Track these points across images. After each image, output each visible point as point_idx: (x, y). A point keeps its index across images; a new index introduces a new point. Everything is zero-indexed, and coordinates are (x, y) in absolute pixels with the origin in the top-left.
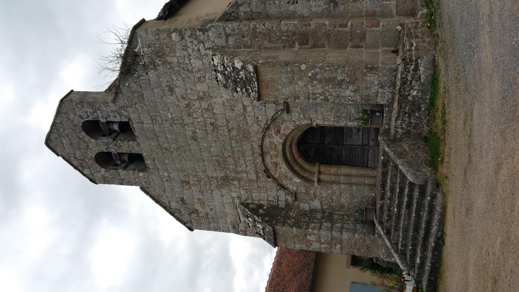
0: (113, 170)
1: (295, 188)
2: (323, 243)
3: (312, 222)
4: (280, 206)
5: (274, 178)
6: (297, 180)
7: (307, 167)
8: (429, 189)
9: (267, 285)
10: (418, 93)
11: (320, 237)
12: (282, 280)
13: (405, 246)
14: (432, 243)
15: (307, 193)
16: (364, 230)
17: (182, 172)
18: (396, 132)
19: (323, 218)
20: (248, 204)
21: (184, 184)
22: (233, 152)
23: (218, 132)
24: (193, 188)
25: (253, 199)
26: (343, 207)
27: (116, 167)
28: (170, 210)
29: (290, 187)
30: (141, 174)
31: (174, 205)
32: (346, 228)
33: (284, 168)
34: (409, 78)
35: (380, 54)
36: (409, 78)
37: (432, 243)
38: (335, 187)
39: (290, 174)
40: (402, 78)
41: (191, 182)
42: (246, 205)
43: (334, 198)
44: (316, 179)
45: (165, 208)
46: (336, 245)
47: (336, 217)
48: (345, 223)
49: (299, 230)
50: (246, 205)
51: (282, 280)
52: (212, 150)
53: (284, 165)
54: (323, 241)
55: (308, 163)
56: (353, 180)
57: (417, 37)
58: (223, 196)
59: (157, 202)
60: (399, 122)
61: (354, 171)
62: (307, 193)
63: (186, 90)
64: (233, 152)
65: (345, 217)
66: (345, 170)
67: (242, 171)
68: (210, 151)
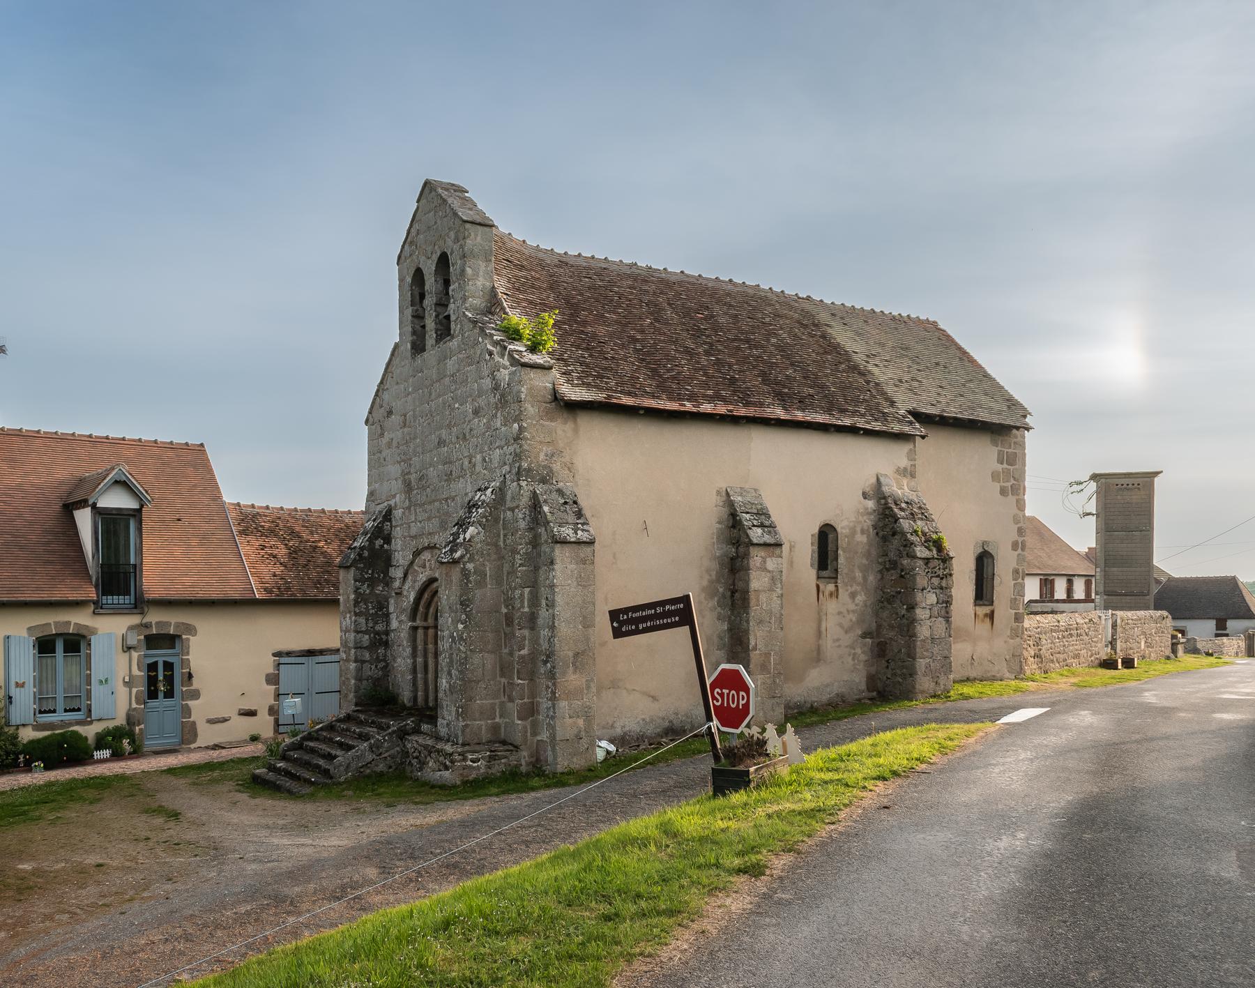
0: (411, 297)
3: (367, 620)
4: (390, 568)
8: (1053, 739)
13: (312, 751)
19: (378, 633)
20: (390, 520)
25: (396, 527)
26: (394, 659)
29: (406, 587)
31: (386, 396)
32: (362, 667)
38: (409, 650)
39: (418, 585)
41: (406, 430)
44: (418, 622)
47: (381, 651)
52: (432, 469)
58: (396, 480)
65: (383, 664)
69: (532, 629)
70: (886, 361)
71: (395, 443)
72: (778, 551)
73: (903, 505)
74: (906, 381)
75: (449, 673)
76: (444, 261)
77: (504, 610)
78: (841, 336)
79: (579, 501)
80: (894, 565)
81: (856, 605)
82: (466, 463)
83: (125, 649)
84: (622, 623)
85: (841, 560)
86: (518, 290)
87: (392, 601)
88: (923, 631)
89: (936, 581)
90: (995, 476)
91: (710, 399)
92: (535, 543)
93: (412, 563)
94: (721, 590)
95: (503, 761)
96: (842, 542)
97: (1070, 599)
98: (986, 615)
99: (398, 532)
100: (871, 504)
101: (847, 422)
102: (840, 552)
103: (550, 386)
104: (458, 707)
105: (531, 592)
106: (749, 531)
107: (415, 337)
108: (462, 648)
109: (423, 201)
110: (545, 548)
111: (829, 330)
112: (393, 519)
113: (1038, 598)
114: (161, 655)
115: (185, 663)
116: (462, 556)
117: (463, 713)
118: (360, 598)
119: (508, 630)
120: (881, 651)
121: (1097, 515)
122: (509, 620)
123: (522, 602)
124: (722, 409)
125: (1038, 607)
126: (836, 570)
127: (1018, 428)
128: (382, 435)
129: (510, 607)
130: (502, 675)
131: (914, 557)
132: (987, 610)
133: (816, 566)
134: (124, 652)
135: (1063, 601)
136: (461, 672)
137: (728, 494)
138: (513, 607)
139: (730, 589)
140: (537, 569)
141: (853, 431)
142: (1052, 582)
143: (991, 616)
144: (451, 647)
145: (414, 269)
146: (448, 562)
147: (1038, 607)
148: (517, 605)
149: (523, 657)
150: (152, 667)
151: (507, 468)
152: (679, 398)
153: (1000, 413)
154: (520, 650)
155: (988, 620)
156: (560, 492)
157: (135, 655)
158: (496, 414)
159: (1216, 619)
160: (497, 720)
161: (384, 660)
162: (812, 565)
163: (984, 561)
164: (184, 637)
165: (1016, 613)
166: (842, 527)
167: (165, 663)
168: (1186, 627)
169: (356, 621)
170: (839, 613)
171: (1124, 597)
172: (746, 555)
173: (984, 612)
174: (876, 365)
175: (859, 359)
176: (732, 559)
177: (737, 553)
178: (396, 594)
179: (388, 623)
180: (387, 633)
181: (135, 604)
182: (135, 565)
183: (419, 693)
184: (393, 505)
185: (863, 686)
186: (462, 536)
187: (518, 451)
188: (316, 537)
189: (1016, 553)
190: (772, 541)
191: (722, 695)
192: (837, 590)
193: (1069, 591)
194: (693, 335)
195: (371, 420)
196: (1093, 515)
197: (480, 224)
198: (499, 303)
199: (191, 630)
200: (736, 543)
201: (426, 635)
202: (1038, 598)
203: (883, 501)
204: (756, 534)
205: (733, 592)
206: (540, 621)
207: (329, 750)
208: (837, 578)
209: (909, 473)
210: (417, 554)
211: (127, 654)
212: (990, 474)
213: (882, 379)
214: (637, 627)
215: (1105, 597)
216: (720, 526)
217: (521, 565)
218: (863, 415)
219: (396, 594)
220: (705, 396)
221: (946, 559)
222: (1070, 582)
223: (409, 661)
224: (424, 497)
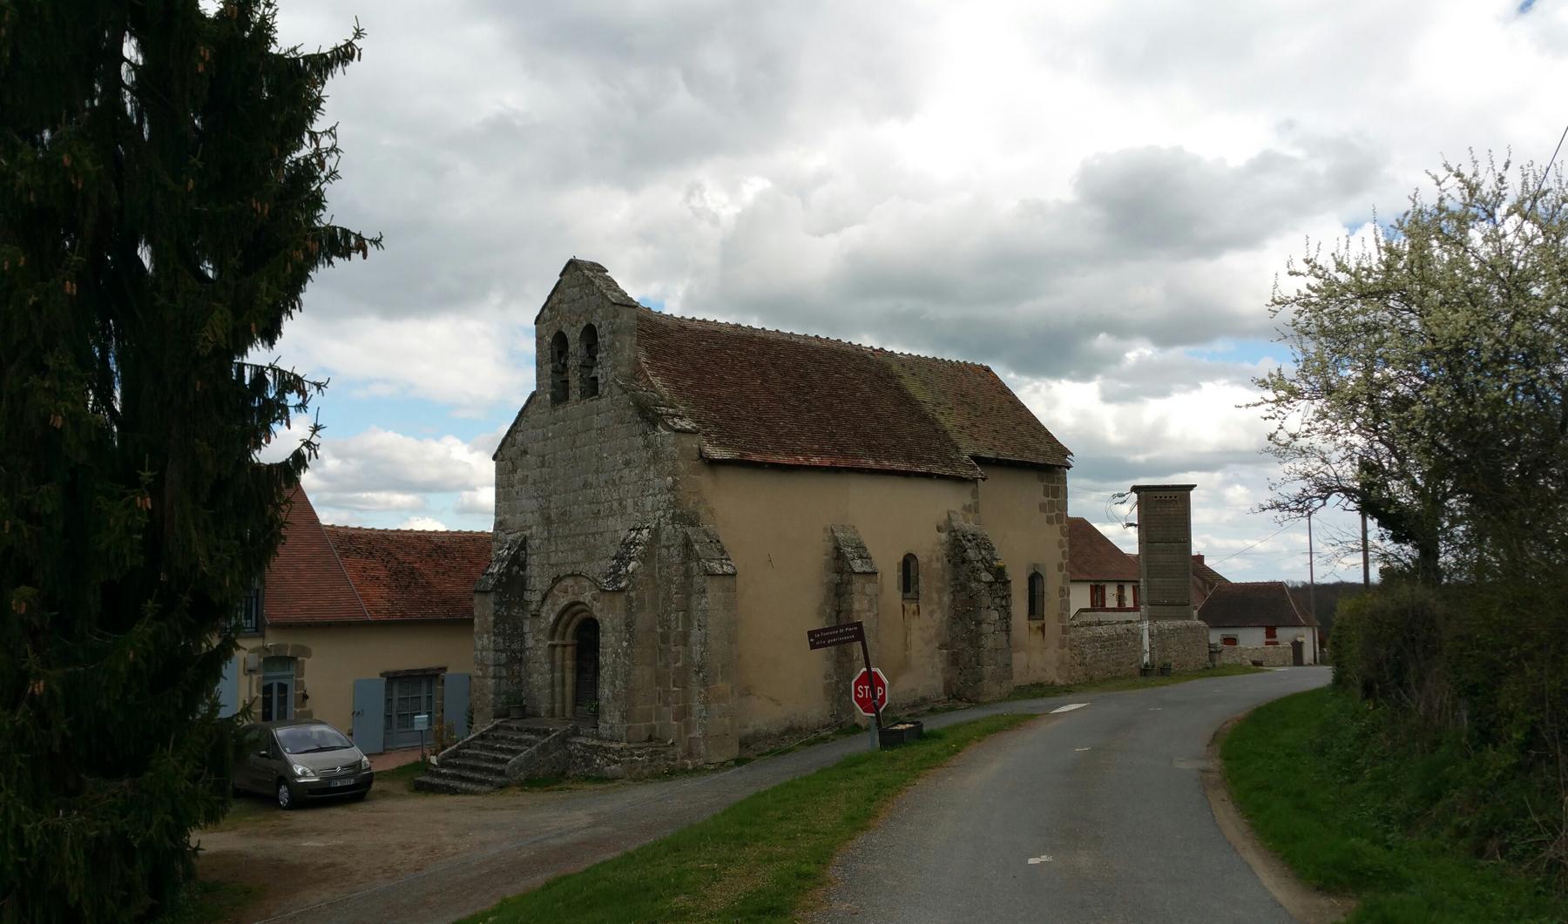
1: (544, 615)
2: (481, 653)
5: (552, 588)
6: (552, 618)
7: (570, 630)
9: (465, 532)
10: (598, 764)
11: (487, 650)
12: (471, 562)
13: (464, 756)
14: (453, 783)
15: (540, 631)
16: (499, 705)
17: (554, 459)
18: (571, 744)
19: (513, 651)
20: (525, 549)
21: (541, 458)
22: (574, 536)
23: (592, 518)
24: (538, 470)
25: (531, 555)
26: (530, 676)
27: (556, 356)
28: (513, 431)
29: (545, 609)
30: (548, 396)
31: (519, 437)
33: (563, 602)
34: (609, 755)
35: (663, 722)
36: (609, 755)
37: (453, 783)
38: (547, 667)
39: (558, 609)
40: (609, 748)
41: (544, 470)
42: (523, 545)
43: (537, 665)
44: (556, 641)
45: (515, 424)
46: (481, 670)
47: (516, 667)
48: (508, 680)
49: (492, 624)
50: (523, 545)
51: (471, 562)
52: (576, 507)
53: (566, 603)
54: (484, 653)
55: (575, 630)
56: (558, 689)
57: (652, 761)
58: (532, 512)
59: (521, 413)
60: (579, 746)
61: (569, 689)
62: (540, 631)
63: (628, 484)
64: (574, 536)
65: (518, 679)
66: (570, 678)
67: (557, 545)
68: (574, 504)
69: (685, 645)
70: (950, 408)
71: (530, 480)
72: (874, 578)
73: (970, 537)
74: (967, 427)
75: (613, 684)
76: (590, 333)
77: (659, 630)
78: (913, 387)
79: (721, 540)
80: (964, 587)
81: (934, 621)
82: (615, 504)
83: (247, 672)
84: (817, 640)
85: (921, 584)
86: (656, 359)
87: (527, 622)
88: (988, 643)
89: (997, 601)
90: (1042, 508)
91: (818, 453)
92: (688, 574)
93: (552, 588)
94: (828, 610)
95: (663, 755)
96: (922, 569)
97: (1121, 608)
98: (1038, 628)
99: (534, 560)
100: (944, 536)
101: (923, 469)
102: (920, 577)
103: (696, 446)
104: (623, 712)
105: (684, 615)
106: (851, 562)
107: (554, 390)
108: (626, 662)
109: (566, 277)
110: (698, 580)
111: (903, 381)
112: (528, 548)
113: (1089, 607)
114: (277, 673)
115: (300, 685)
116: (627, 586)
117: (626, 716)
118: (499, 620)
119: (663, 646)
120: (954, 660)
121: (1139, 526)
122: (665, 638)
123: (677, 623)
124: (827, 463)
125: (1090, 617)
126: (918, 592)
127: (1060, 467)
128: (514, 471)
129: (666, 628)
130: (658, 684)
131: (979, 581)
132: (1039, 623)
133: (902, 588)
134: (246, 675)
135: (1113, 610)
136: (626, 682)
137: (832, 531)
138: (669, 628)
139: (836, 611)
140: (688, 596)
141: (928, 476)
142: (1103, 589)
143: (1042, 629)
144: (614, 662)
145: (555, 332)
146: (613, 591)
147: (1090, 617)
148: (673, 625)
149: (678, 668)
150: (267, 690)
151: (661, 513)
152: (793, 453)
153: (1044, 454)
154: (676, 663)
155: (1040, 632)
156: (706, 533)
157: (255, 677)
158: (649, 467)
159: (1266, 627)
160: (653, 722)
161: (519, 676)
162: (898, 588)
163: (1035, 579)
164: (300, 659)
165: (1063, 626)
166: (922, 558)
167: (279, 684)
168: (1237, 635)
169: (495, 641)
170: (920, 629)
171: (1166, 607)
172: (849, 582)
173: (1037, 625)
174: (942, 414)
175: (928, 408)
176: (837, 585)
177: (841, 580)
178: (533, 615)
179: (523, 642)
180: (522, 651)
181: (256, 628)
182: (258, 590)
183: (557, 705)
184: (528, 535)
185: (941, 690)
186: (624, 569)
187: (672, 500)
188: (411, 558)
189: (1062, 573)
190: (868, 570)
191: (864, 690)
192: (919, 609)
193: (1121, 598)
194: (795, 393)
195: (500, 456)
196: (1135, 525)
197: (627, 306)
198: (642, 371)
199: (307, 652)
200: (840, 571)
201: (564, 652)
202: (1089, 607)
203: (953, 534)
204: (858, 566)
205: (839, 613)
206: (692, 639)
207: (493, 755)
208: (918, 599)
209: (973, 509)
210: (557, 580)
211: (248, 677)
212: (1038, 506)
213: (948, 426)
214: (827, 641)
215: (1149, 607)
216: (826, 557)
217: (676, 593)
218: (936, 462)
219: (533, 615)
220: (812, 450)
221: (1006, 583)
222: (1121, 589)
223: (548, 676)
224: (567, 532)
